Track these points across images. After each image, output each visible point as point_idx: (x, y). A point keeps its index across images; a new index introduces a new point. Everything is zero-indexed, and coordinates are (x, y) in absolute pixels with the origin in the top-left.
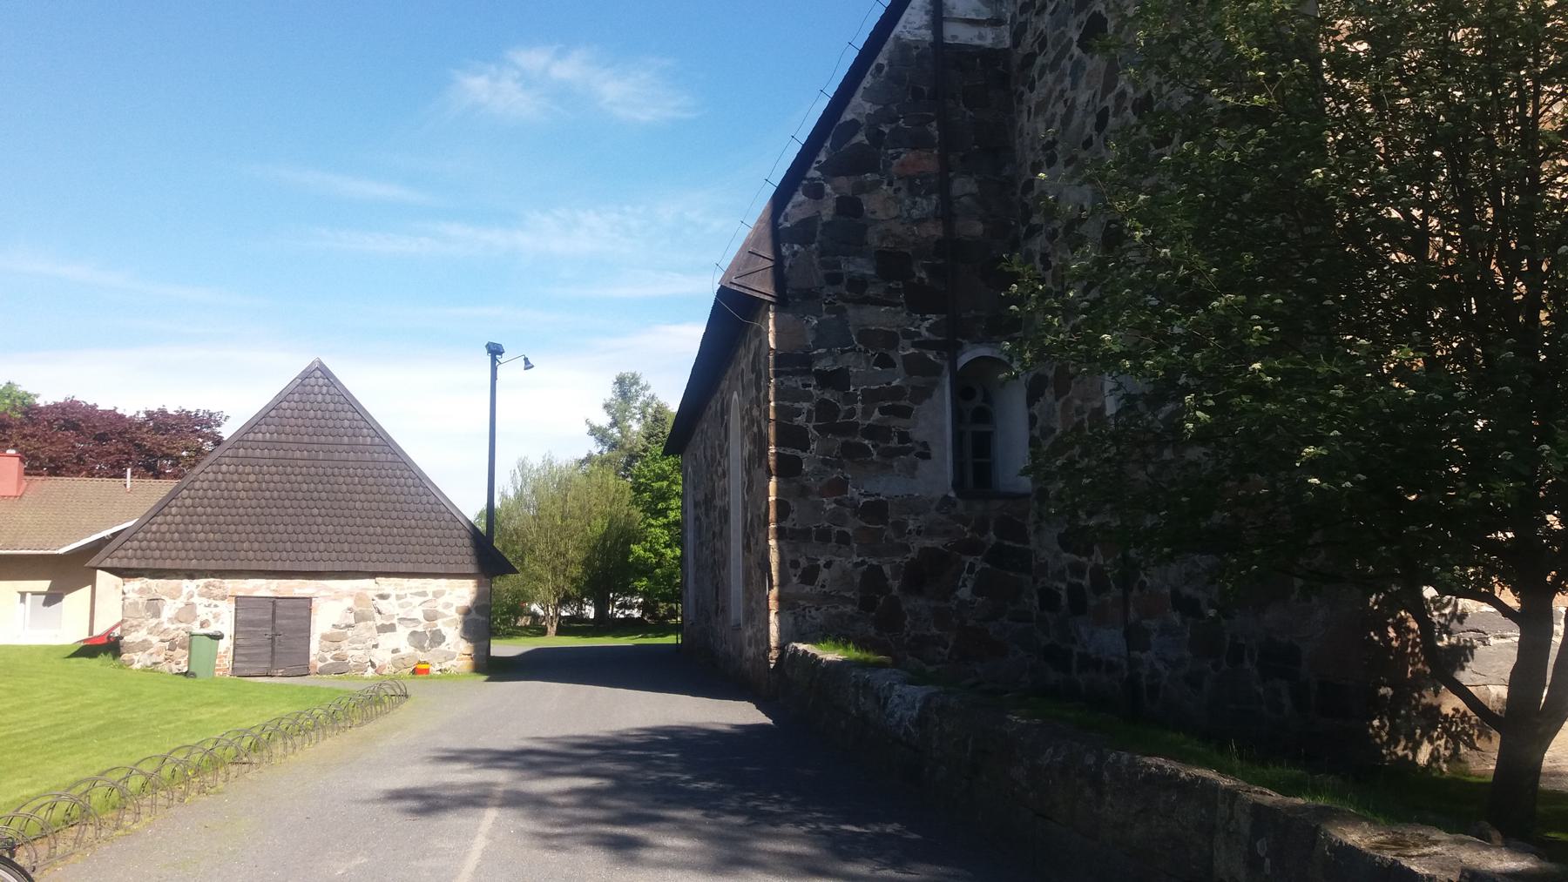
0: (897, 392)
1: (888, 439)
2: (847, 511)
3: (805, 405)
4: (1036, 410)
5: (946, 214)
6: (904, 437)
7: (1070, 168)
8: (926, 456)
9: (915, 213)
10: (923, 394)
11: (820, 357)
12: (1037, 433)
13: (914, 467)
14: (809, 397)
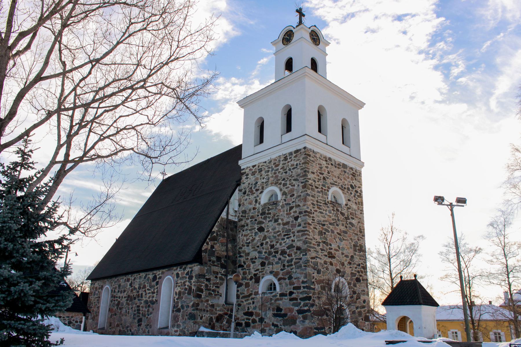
0: (218, 283)
1: (215, 292)
2: (208, 306)
3: (203, 285)
4: (239, 289)
5: (227, 251)
6: (218, 292)
7: (253, 249)
8: (221, 296)
9: (222, 250)
10: (221, 284)
11: (207, 275)
12: (239, 293)
13: (219, 298)
14: (204, 283)
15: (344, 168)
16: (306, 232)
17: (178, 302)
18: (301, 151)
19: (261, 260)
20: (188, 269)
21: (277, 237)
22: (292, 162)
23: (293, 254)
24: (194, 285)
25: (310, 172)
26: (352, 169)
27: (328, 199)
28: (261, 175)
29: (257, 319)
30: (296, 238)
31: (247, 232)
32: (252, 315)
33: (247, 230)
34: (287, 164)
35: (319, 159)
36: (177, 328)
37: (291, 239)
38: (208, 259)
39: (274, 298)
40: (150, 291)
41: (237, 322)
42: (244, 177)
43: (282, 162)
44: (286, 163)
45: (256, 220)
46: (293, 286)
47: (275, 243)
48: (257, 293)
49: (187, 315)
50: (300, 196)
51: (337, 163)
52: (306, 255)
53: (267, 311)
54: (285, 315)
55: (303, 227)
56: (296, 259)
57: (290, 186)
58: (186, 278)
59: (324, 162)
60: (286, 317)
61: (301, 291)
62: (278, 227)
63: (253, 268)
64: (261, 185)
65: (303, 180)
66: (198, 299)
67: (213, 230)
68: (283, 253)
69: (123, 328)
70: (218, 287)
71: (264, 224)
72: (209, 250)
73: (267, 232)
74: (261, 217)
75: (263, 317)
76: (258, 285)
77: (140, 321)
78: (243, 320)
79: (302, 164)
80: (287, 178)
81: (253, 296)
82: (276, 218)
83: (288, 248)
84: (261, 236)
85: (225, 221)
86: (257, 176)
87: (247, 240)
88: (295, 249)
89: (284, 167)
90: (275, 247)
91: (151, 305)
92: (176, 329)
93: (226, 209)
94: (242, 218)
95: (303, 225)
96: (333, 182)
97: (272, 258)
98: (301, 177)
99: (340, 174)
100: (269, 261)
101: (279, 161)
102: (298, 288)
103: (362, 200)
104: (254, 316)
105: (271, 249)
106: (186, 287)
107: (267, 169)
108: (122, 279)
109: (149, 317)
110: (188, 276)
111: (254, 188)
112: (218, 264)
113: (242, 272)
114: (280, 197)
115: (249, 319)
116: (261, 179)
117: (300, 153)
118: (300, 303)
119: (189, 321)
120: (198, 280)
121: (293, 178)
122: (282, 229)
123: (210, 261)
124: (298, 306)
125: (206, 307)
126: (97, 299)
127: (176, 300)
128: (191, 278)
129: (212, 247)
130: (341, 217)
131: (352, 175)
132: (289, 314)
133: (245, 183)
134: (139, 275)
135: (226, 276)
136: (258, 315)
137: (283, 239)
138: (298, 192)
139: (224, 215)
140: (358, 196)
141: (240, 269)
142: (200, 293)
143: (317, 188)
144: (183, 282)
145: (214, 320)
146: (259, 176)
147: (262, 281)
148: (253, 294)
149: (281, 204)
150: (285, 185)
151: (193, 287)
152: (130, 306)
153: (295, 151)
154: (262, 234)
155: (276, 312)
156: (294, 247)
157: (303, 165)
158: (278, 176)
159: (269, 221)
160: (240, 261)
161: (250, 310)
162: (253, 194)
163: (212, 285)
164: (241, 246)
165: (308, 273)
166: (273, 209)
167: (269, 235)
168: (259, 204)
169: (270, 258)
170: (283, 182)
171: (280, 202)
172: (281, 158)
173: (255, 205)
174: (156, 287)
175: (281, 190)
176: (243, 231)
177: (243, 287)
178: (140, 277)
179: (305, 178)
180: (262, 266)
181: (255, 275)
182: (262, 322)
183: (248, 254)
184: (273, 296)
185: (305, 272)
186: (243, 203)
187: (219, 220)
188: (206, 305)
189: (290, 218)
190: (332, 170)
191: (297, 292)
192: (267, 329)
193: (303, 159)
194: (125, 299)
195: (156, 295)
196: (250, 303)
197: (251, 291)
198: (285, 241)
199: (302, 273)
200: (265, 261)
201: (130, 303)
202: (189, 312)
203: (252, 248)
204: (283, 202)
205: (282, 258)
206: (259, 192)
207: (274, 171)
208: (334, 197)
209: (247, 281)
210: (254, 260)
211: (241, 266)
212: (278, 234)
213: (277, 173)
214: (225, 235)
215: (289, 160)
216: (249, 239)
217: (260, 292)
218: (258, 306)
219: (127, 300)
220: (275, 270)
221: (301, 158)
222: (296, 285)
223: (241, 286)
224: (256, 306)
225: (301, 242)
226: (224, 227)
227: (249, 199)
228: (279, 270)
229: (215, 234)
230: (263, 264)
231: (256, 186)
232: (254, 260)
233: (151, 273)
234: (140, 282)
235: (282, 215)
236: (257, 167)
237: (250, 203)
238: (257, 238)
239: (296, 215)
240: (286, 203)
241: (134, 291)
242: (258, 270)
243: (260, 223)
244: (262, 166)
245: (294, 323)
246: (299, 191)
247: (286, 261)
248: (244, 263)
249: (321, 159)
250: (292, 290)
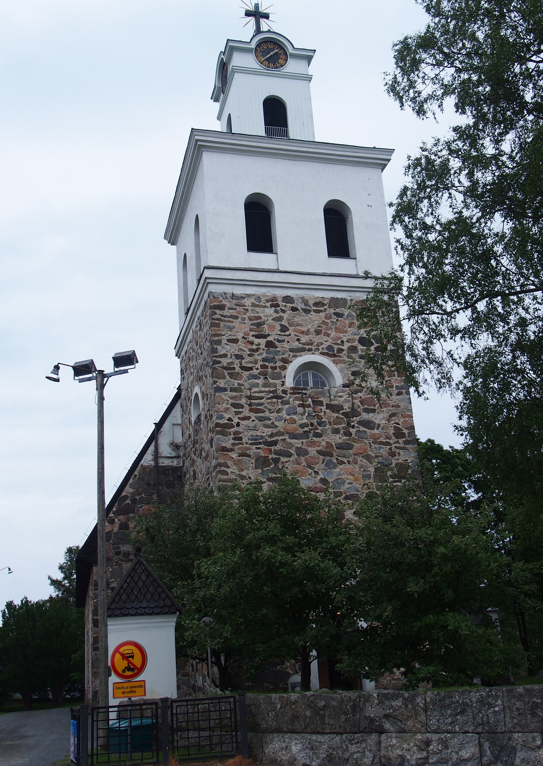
25: (224, 341)
51: (311, 303)
59: (270, 311)
67: (124, 494)
96: (301, 346)
123: (118, 553)
130: (328, 415)
187: (136, 473)
229: (128, 501)
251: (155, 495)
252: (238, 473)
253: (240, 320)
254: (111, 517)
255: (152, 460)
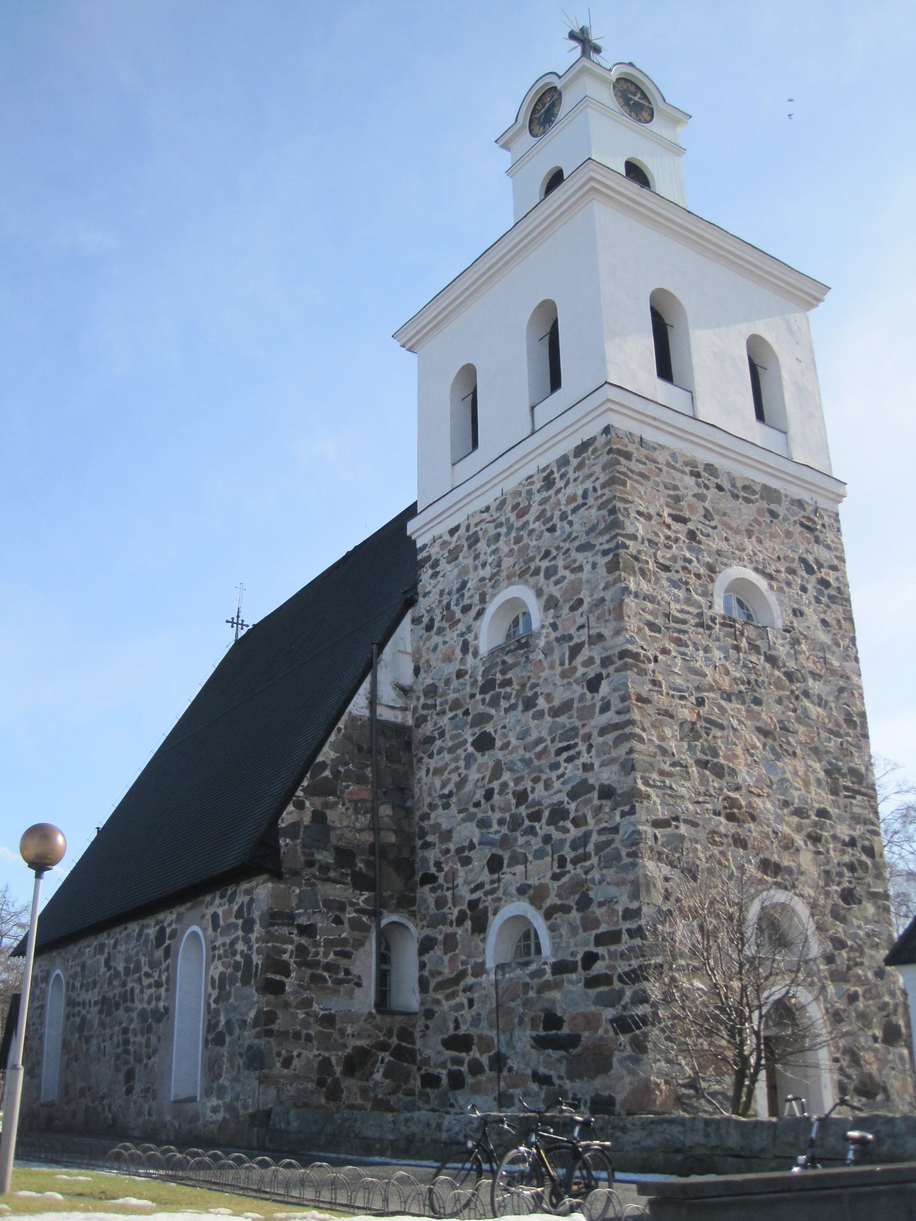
0: (344, 942)
1: (337, 973)
2: (312, 1020)
3: (290, 947)
4: (426, 958)
5: (375, 827)
6: (347, 972)
7: (462, 815)
8: (359, 985)
9: (358, 825)
10: (359, 944)
11: (300, 915)
12: (426, 973)
13: (352, 991)
14: (291, 942)
15: (770, 501)
16: (628, 730)
17: (217, 1011)
18: (597, 444)
19: (488, 852)
20: (241, 899)
21: (536, 763)
22: (570, 490)
23: (589, 816)
24: (259, 951)
25: (633, 515)
26: (800, 503)
27: (710, 607)
28: (477, 557)
29: (485, 1060)
30: (598, 756)
31: (443, 759)
32: (468, 1049)
33: (440, 751)
34: (552, 500)
35: (665, 468)
36: (218, 1098)
37: (579, 762)
38: (302, 859)
39: (535, 982)
40: (151, 980)
41: (423, 1072)
42: (426, 575)
43: (537, 497)
44: (549, 498)
45: (466, 713)
46: (594, 933)
47: (528, 784)
48: (480, 970)
49: (241, 1055)
50: (603, 600)
51: (739, 484)
52: (632, 812)
53: (513, 1029)
54: (573, 1040)
55: (618, 713)
56: (601, 831)
57: (567, 573)
58: (235, 926)
59: (690, 481)
60: (575, 1047)
61: (622, 947)
62: (537, 726)
63: (466, 882)
64: (477, 589)
65: (608, 541)
66: (271, 997)
67: (320, 758)
68: (558, 814)
69: (93, 1102)
70: (348, 955)
71: (491, 724)
72: (307, 827)
73: (502, 748)
74: (483, 700)
75: (504, 1050)
76: (484, 940)
77: (130, 1076)
78: (443, 1065)
79: (603, 486)
80: (558, 548)
81: (470, 980)
82: (529, 694)
83: (573, 795)
84: (486, 764)
85: (363, 726)
86: (466, 562)
87: (443, 786)
88: (595, 794)
89: (544, 510)
90: (531, 797)
91: (154, 1026)
92: (214, 1101)
93: (366, 685)
94: (425, 712)
95: (616, 704)
97: (521, 840)
98: (601, 534)
99: (755, 520)
100: (514, 852)
101: (530, 493)
102: (613, 937)
103: (850, 612)
104: (475, 1048)
105: (517, 806)
106: (238, 958)
107: (492, 532)
108: (89, 946)
109: (150, 1063)
110: (240, 922)
111: (457, 604)
112: (343, 875)
113: (431, 899)
114: (537, 617)
115: (460, 1062)
116: (476, 568)
117: (594, 451)
118: (620, 994)
119: (246, 1073)
120: (267, 932)
121: (577, 543)
122: (551, 730)
123: (310, 864)
124: (613, 1006)
125: (305, 1024)
126: (38, 1012)
127: (213, 1006)
128: (248, 927)
129: (319, 817)
131: (802, 525)
132: (585, 1034)
133: (429, 593)
134: (126, 929)
135: (376, 914)
136: (486, 1044)
137: (555, 766)
138: (593, 590)
139: (358, 705)
140: (831, 598)
141: (428, 887)
142: (278, 977)
143: (666, 569)
144: (228, 941)
145: (338, 1070)
146: (470, 561)
147: (495, 924)
148: (470, 971)
149: (542, 643)
150: (550, 572)
151: (257, 959)
152: (108, 1031)
153: (577, 448)
154: (486, 759)
155: (542, 1033)
156: (591, 788)
157: (606, 491)
158: (527, 546)
159: (507, 710)
160: (425, 860)
161: (463, 1030)
162: (454, 623)
163: (322, 949)
164: (426, 809)
165: (641, 880)
166: (519, 663)
167: (510, 758)
168: (476, 654)
169: (516, 840)
170: (545, 564)
171: (539, 635)
172: (532, 483)
173: (463, 661)
174: (164, 965)
175: (539, 593)
176: (431, 756)
177: (438, 951)
178: (128, 936)
179: (617, 535)
180: (492, 871)
181: (473, 904)
182: (500, 1071)
183: (447, 836)
184: (532, 975)
185: (631, 877)
186: (427, 661)
187: (341, 724)
188: (302, 1016)
189: (575, 686)
190: (722, 505)
191: (609, 953)
192: (517, 1092)
193: (604, 468)
194: (97, 1008)
195: (167, 990)
196: (460, 1006)
197: (463, 963)
198: (560, 771)
199: (623, 883)
200: (500, 852)
201: (108, 1019)
202: (246, 1044)
203: (460, 812)
204: (547, 637)
205: (556, 835)
206: (473, 613)
207: (513, 534)
208: (886, 798)
209: (449, 930)
210: (466, 853)
211: (429, 879)
212: (539, 749)
213: (525, 536)
214: (365, 776)
215: (559, 484)
216: (449, 780)
217: (490, 964)
218: (484, 1014)
219: (100, 1012)
220: (534, 881)
221: (597, 469)
222: (603, 928)
223: (432, 948)
224: (479, 1015)
225: (615, 768)
226: (360, 749)
227: (445, 643)
228: (547, 880)
229: (327, 773)
230: (495, 864)
231: (462, 596)
232: (466, 853)
233: (151, 921)
234: (127, 951)
235: (546, 680)
236: (462, 530)
237: (448, 659)
238: (474, 776)
239: (592, 672)
240: (558, 634)
241: (116, 983)
242: (480, 886)
243: (483, 719)
244: (477, 525)
245: (604, 1066)
246: (597, 585)
247: (568, 844)
248: (438, 865)
249: (674, 468)
250: (592, 948)
251: (369, 769)
252: (657, 742)
253: (651, 483)
254: (299, 797)
255: (367, 708)
